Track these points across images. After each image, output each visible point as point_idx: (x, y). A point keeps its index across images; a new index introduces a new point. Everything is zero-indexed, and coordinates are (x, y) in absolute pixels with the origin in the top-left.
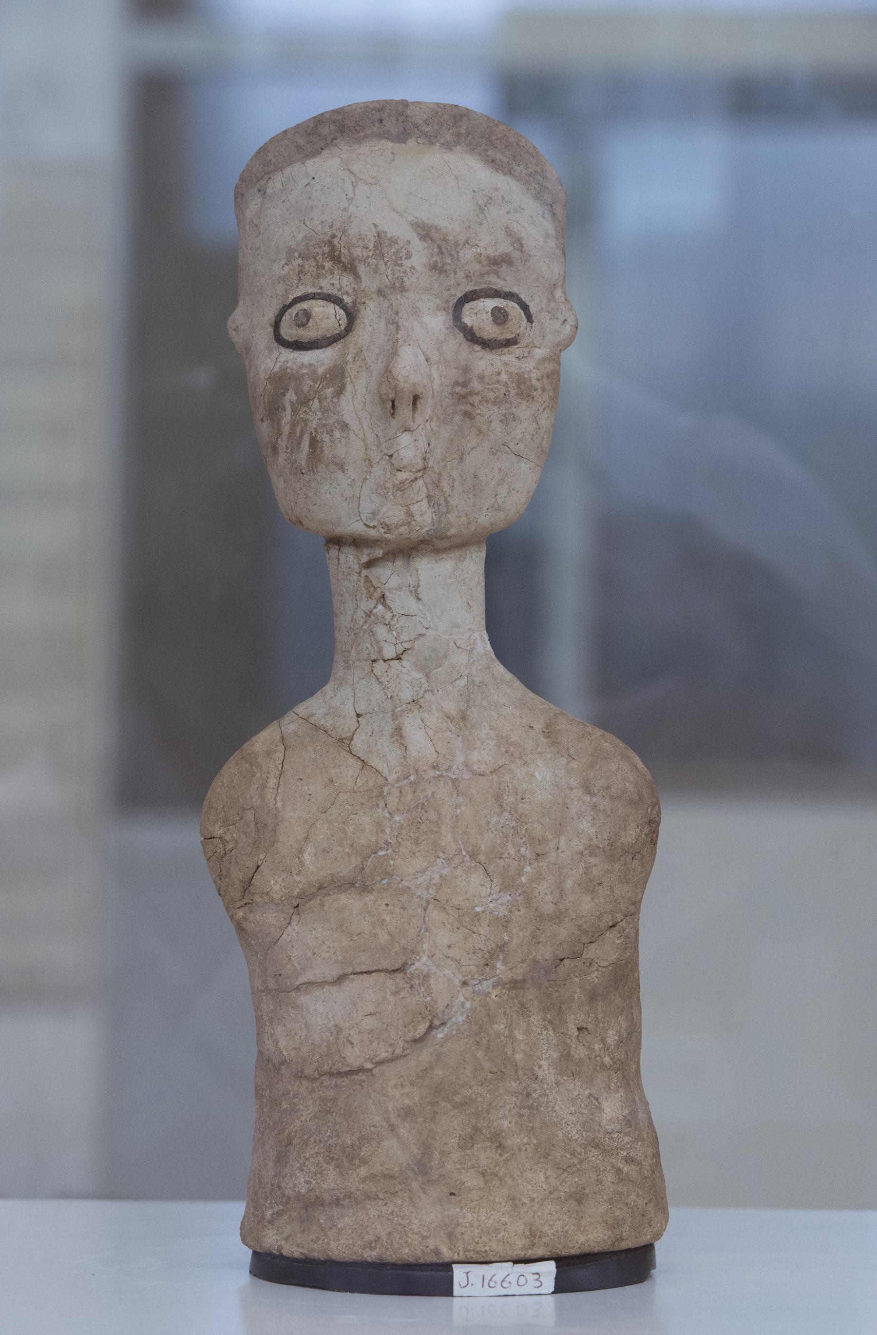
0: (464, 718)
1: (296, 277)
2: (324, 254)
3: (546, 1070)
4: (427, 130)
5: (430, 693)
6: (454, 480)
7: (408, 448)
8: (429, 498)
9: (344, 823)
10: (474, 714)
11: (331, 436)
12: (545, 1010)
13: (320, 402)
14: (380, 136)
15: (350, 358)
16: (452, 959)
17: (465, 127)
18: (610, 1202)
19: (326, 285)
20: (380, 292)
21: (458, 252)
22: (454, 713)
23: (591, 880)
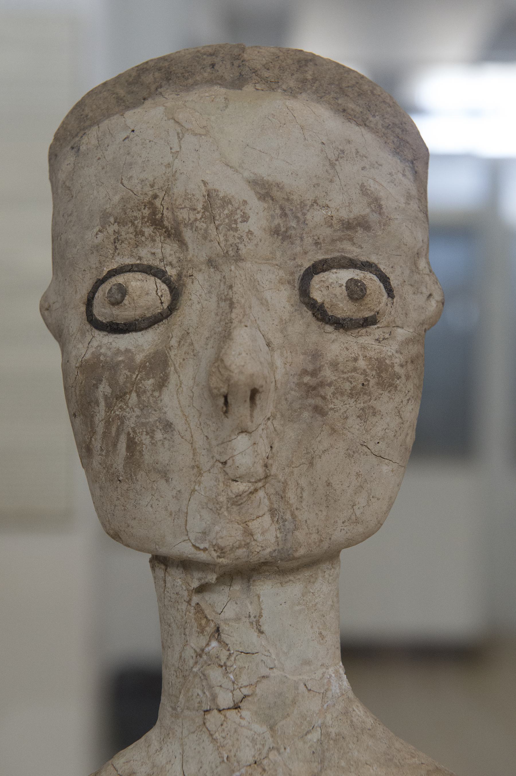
1: (111, 246)
2: (143, 218)
4: (266, 75)
5: (276, 752)
6: (302, 489)
7: (245, 453)
8: (272, 511)
11: (152, 437)
13: (138, 396)
14: (211, 82)
15: (174, 342)
17: (310, 73)
19: (146, 255)
20: (211, 263)
21: (304, 214)
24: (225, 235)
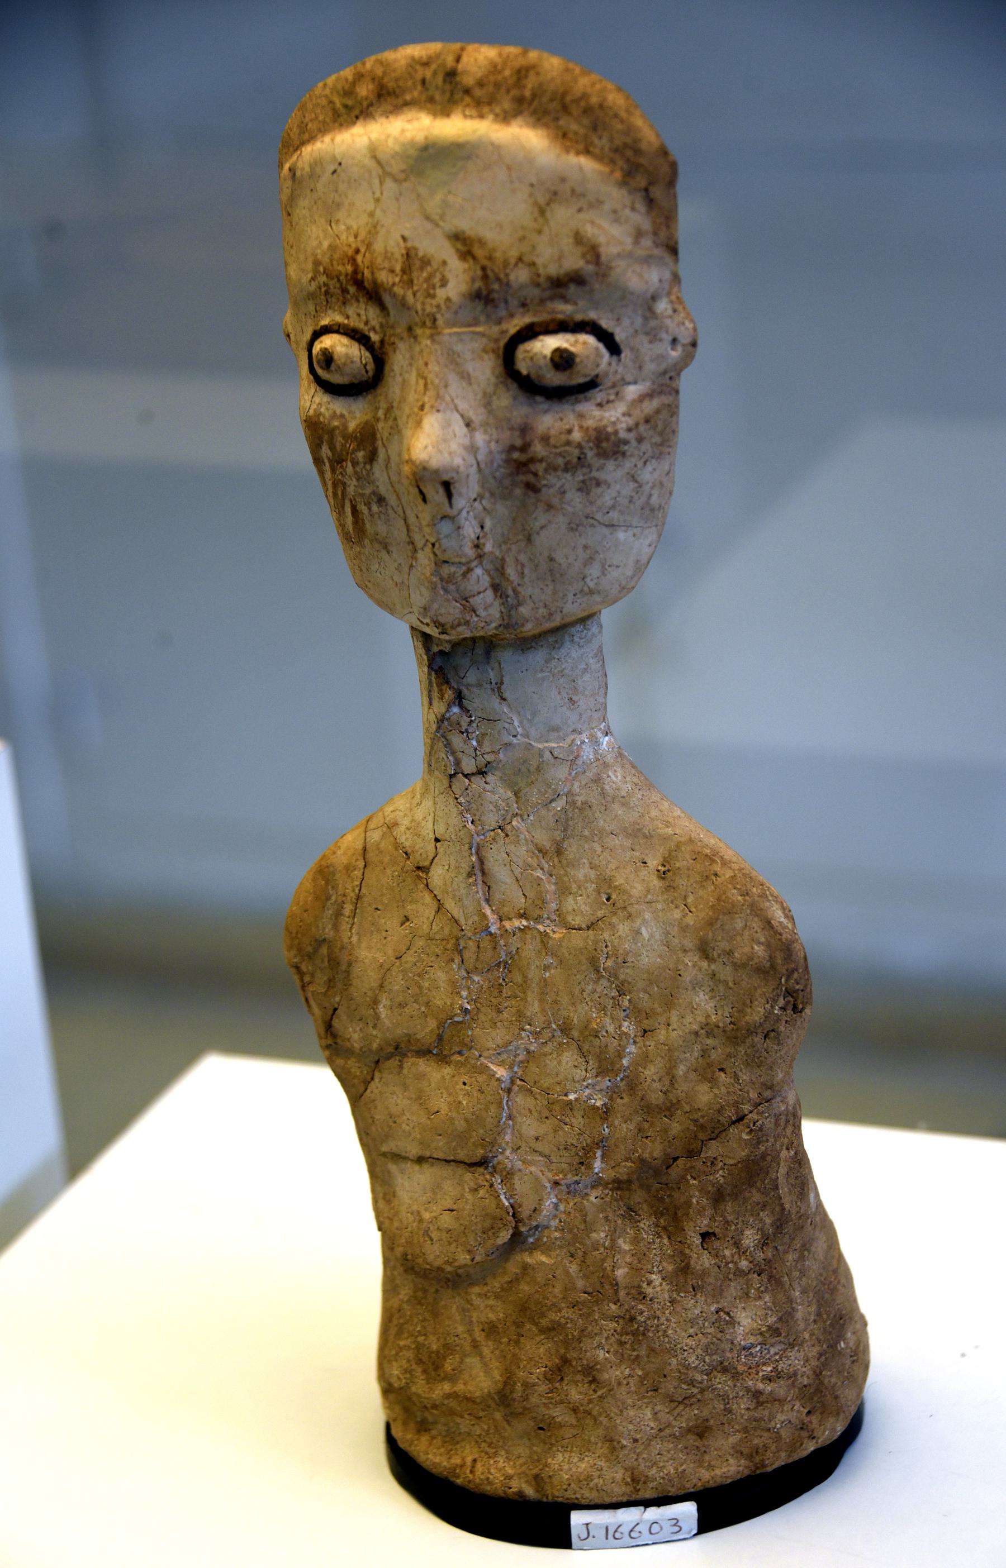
0: (559, 852)
2: (347, 275)
3: (657, 1286)
8: (496, 587)
9: (419, 975)
10: (572, 849)
12: (658, 1214)
15: (381, 414)
16: (541, 1154)
18: (745, 1430)
21: (507, 275)
22: (547, 845)
23: (709, 1065)
24: (423, 304)
